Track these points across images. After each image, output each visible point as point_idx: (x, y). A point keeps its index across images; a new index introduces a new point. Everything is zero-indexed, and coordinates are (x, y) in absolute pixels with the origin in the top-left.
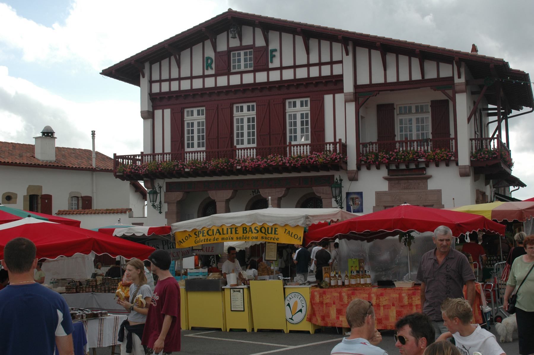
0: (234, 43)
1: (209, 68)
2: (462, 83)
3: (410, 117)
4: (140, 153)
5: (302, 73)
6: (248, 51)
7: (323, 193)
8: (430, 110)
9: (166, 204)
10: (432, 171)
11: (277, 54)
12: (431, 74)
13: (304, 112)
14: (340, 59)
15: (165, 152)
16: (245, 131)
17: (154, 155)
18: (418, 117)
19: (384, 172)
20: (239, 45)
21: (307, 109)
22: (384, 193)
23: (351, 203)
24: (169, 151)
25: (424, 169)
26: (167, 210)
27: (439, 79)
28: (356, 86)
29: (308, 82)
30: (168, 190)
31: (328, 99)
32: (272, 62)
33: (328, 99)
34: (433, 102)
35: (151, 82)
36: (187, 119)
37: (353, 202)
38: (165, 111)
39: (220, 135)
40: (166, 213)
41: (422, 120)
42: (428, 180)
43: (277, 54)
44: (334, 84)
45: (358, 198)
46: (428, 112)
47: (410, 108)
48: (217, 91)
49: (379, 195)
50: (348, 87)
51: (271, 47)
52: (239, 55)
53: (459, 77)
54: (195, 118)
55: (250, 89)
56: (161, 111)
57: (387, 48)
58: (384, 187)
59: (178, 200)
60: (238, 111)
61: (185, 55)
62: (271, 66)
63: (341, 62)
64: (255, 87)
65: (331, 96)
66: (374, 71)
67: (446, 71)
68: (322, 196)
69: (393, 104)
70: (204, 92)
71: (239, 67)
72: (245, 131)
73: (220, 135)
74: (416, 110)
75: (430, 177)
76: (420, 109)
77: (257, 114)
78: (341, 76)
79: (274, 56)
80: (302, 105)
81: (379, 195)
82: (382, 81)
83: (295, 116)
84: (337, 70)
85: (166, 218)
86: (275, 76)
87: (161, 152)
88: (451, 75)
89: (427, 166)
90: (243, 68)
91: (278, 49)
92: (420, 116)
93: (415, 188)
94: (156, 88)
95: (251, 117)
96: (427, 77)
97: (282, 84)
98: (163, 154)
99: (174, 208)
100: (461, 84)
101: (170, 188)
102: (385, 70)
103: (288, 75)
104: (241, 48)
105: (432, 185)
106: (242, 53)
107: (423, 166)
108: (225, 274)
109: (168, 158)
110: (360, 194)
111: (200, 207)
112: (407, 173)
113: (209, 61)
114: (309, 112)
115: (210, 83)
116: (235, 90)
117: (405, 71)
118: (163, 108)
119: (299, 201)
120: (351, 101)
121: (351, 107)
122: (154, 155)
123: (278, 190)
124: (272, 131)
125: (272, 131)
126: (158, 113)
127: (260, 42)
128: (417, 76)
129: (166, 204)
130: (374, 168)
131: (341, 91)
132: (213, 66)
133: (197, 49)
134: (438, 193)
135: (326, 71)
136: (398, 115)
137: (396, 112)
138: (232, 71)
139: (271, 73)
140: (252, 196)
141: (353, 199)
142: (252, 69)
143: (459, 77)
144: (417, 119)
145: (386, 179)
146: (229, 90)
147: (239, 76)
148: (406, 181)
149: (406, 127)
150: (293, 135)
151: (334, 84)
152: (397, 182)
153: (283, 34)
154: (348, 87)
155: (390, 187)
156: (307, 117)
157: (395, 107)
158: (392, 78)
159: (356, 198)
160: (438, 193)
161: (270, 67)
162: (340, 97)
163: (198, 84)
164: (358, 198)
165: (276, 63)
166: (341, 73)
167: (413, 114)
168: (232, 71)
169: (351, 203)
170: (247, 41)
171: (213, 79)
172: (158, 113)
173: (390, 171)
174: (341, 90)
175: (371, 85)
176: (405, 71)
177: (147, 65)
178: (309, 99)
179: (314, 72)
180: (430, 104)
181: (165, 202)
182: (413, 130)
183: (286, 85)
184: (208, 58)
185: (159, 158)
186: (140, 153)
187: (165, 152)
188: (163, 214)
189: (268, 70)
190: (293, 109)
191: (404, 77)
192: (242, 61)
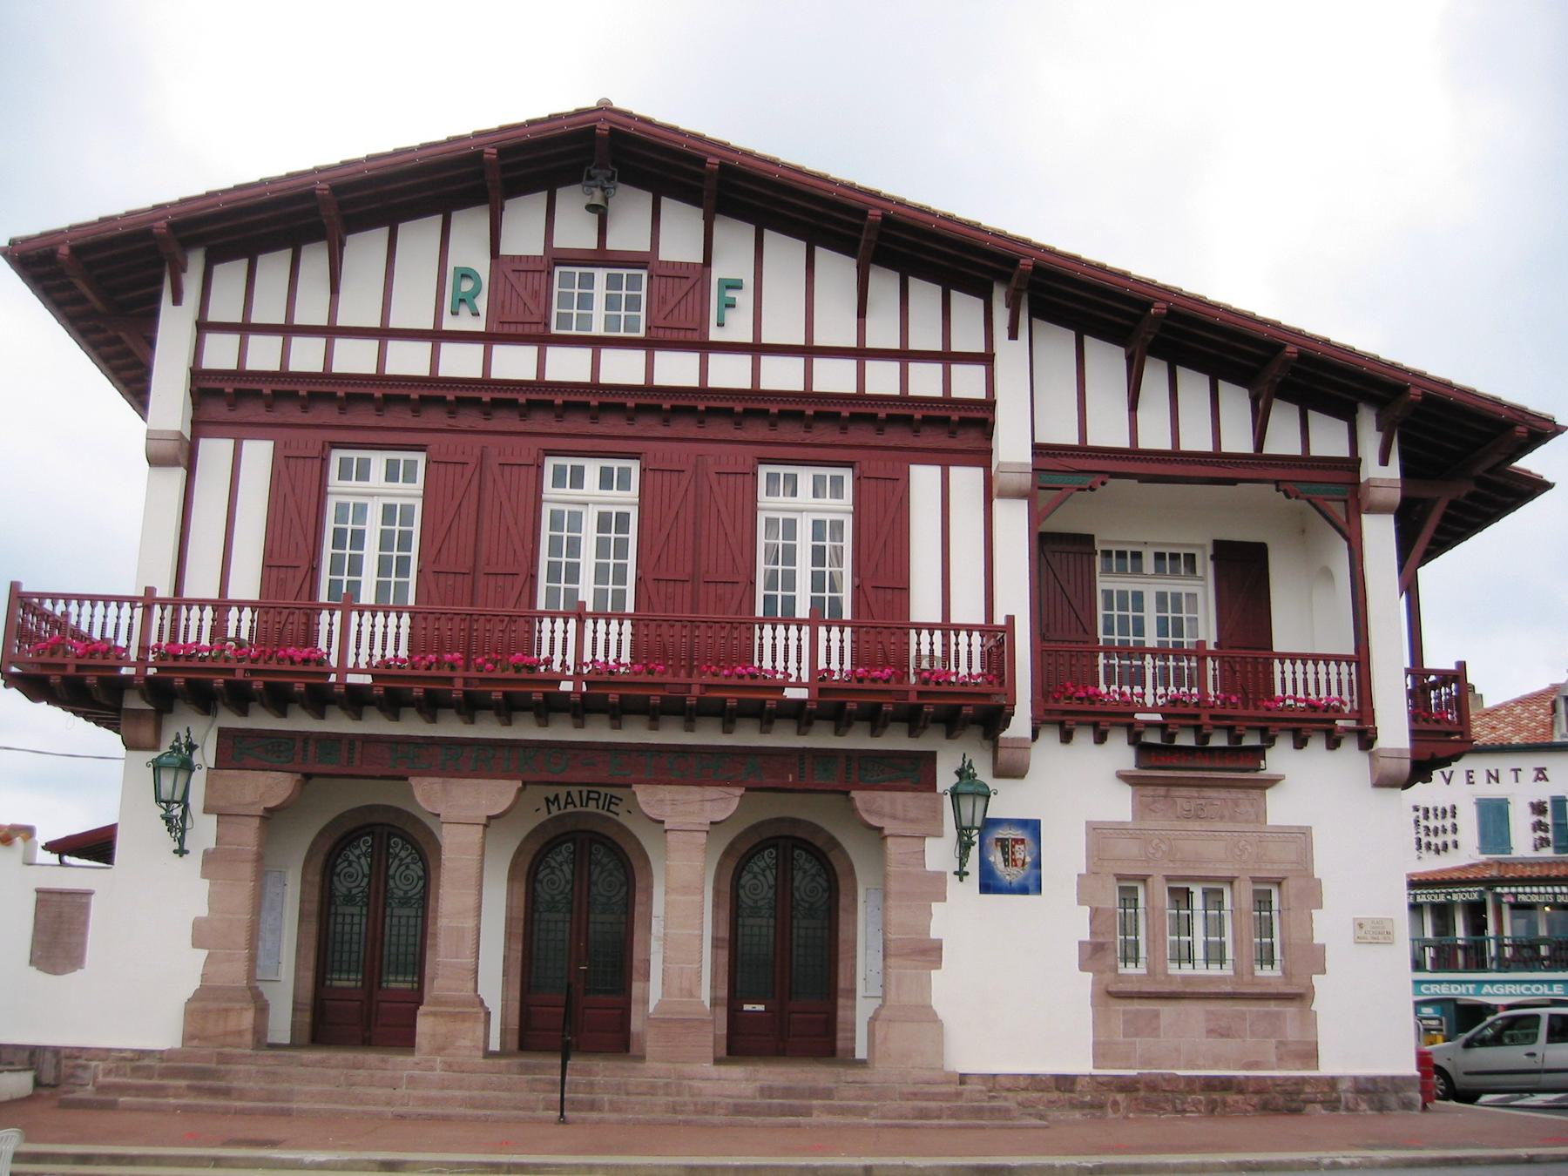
0: (576, 232)
2: (1391, 480)
3: (1138, 588)
5: (835, 377)
6: (625, 272)
7: (894, 817)
9: (214, 818)
10: (1280, 758)
11: (745, 299)
12: (1283, 439)
14: (981, 348)
15: (233, 594)
17: (178, 601)
18: (1162, 588)
19: (1119, 754)
20: (592, 244)
21: (840, 507)
22: (1118, 828)
23: (996, 858)
24: (253, 594)
25: (1258, 753)
26: (211, 844)
27: (1306, 461)
29: (858, 412)
30: (223, 761)
31: (924, 479)
33: (924, 479)
35: (204, 326)
36: (340, 489)
37: (1004, 853)
38: (249, 446)
39: (480, 557)
40: (208, 857)
41: (1177, 597)
42: (1268, 792)
44: (962, 430)
45: (1022, 841)
47: (1137, 556)
49: (1099, 833)
50: (1012, 446)
51: (718, 272)
52: (588, 281)
53: (1384, 461)
54: (378, 493)
56: (227, 445)
58: (1119, 805)
59: (271, 804)
61: (364, 251)
68: (890, 827)
73: (480, 557)
75: (1273, 782)
76: (1176, 562)
78: (989, 405)
79: (731, 305)
81: (1099, 833)
83: (790, 526)
84: (968, 383)
85: (204, 875)
86: (730, 373)
89: (1270, 741)
92: (1170, 586)
93: (1222, 818)
94: (221, 354)
95: (614, 510)
96: (1269, 449)
97: (753, 407)
98: (221, 606)
99: (248, 835)
100: (1387, 484)
101: (234, 752)
102: (1133, 407)
104: (602, 257)
105: (1280, 808)
106: (601, 275)
107: (1251, 740)
109: (241, 624)
110: (1033, 827)
112: (1205, 764)
115: (461, 362)
117: (1199, 417)
118: (239, 430)
119: (732, 845)
122: (178, 601)
123: (712, 792)
124: (695, 568)
125: (695, 568)
126: (215, 452)
128: (1238, 441)
130: (1083, 739)
132: (482, 303)
133: (419, 238)
134: (1301, 837)
135: (926, 381)
140: (543, 816)
141: (1003, 843)
143: (1384, 461)
144: (1161, 598)
145: (1125, 778)
146: (538, 399)
147: (585, 354)
148: (1194, 792)
149: (1123, 620)
152: (1162, 791)
153: (769, 235)
155: (1140, 809)
158: (1155, 437)
159: (1016, 841)
160: (1301, 837)
161: (712, 338)
163: (408, 360)
164: (1022, 841)
165: (738, 328)
166: (980, 394)
167: (1147, 576)
169: (996, 858)
170: (629, 234)
171: (478, 349)
173: (1144, 751)
174: (982, 456)
177: (195, 262)
179: (883, 379)
180: (1210, 551)
181: (206, 810)
184: (465, 274)
185: (197, 628)
187: (233, 594)
188: (194, 861)
189: (707, 348)
191: (1196, 439)
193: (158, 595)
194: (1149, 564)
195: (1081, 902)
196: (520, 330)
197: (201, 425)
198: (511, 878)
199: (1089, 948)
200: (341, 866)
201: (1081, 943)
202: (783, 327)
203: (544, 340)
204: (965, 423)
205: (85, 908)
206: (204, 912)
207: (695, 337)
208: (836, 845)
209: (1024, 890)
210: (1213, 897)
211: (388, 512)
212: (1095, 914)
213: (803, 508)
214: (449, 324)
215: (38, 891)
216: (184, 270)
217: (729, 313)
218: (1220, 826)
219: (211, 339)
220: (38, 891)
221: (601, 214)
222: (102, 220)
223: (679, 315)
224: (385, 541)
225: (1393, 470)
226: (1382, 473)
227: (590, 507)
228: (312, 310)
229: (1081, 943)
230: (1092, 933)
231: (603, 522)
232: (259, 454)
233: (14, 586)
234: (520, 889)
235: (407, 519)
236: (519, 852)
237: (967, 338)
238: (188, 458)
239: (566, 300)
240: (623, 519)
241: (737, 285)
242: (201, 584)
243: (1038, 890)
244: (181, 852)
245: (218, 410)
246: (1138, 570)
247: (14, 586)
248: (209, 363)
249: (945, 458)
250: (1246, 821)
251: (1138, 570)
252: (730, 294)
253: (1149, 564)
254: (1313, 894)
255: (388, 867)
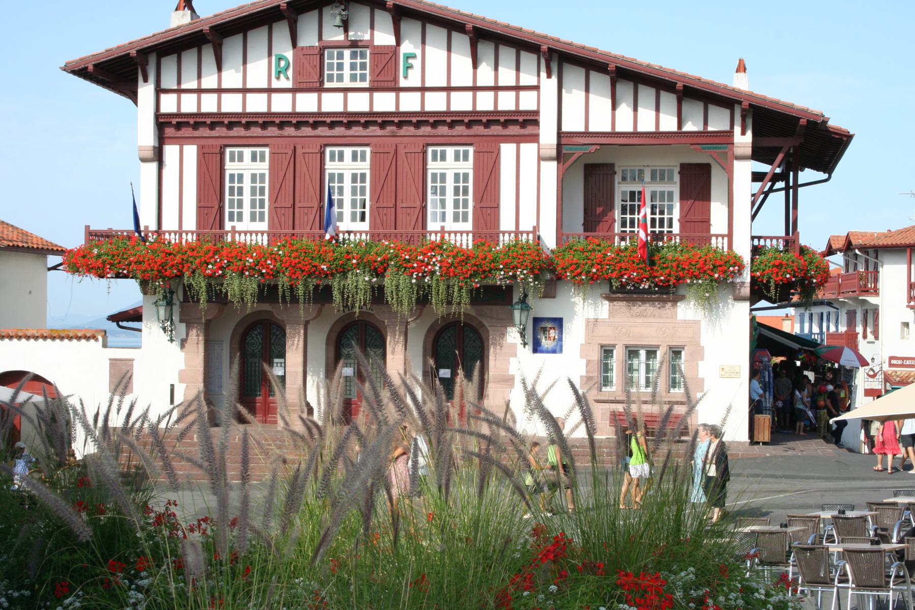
1: (282, 76)
4: (531, 229)
8: (677, 178)
9: (184, 325)
13: (258, 172)
14: (535, 84)
16: (247, 197)
21: (467, 167)
24: (193, 227)
28: (560, 134)
31: (507, 150)
32: (406, 77)
33: (507, 150)
34: (683, 166)
35: (159, 91)
38: (187, 148)
39: (300, 194)
43: (416, 63)
44: (524, 124)
46: (676, 183)
48: (298, 121)
50: (548, 135)
52: (340, 56)
53: (743, 133)
54: (248, 167)
55: (226, 122)
56: (176, 148)
57: (627, 77)
60: (435, 159)
62: (403, 83)
63: (537, 88)
64: (369, 119)
65: (177, 147)
66: (592, 111)
67: (719, 121)
69: (611, 166)
70: (267, 120)
71: (340, 78)
72: (247, 197)
73: (300, 194)
74: (652, 178)
76: (659, 176)
77: (272, 169)
79: (411, 67)
80: (457, 158)
82: (652, 128)
84: (528, 102)
86: (410, 103)
87: (176, 228)
88: (727, 128)
90: (347, 83)
91: (418, 52)
92: (659, 188)
94: (169, 104)
95: (359, 172)
97: (421, 120)
98: (180, 232)
100: (744, 146)
103: (436, 103)
108: (552, 442)
111: (237, 325)
113: (283, 63)
114: (267, 173)
115: (282, 104)
116: (247, 122)
117: (651, 117)
118: (181, 141)
120: (550, 159)
121: (551, 169)
127: (384, 38)
129: (184, 325)
131: (534, 138)
132: (290, 73)
135: (507, 102)
136: (619, 183)
137: (618, 178)
138: (327, 85)
139: (402, 95)
142: (366, 85)
143: (743, 133)
146: (317, 120)
150: (258, 210)
151: (524, 124)
154: (548, 135)
156: (262, 181)
157: (616, 169)
162: (529, 150)
165: (413, 79)
166: (535, 108)
168: (327, 85)
171: (289, 96)
172: (171, 151)
175: (635, 134)
176: (651, 117)
178: (471, 150)
180: (677, 170)
181: (181, 321)
182: (674, 211)
183: (466, 120)
186: (531, 229)
189: (398, 90)
190: (236, 164)
192: (345, 68)
193: (150, 229)
194: (647, 177)
195: (582, 357)
196: (308, 86)
197: (162, 140)
198: (327, 344)
199: (585, 379)
200: (249, 339)
201: (581, 377)
202: (436, 78)
203: (320, 89)
204: (524, 124)
205: (132, 365)
206: (183, 367)
207: (392, 85)
208: (484, 326)
209: (554, 352)
210: (651, 354)
211: (254, 178)
212: (588, 363)
213: (451, 165)
214: (275, 84)
215: (110, 360)
216: (147, 64)
217: (410, 71)
218: (652, 320)
219: (163, 97)
220: (110, 360)
221: (345, 26)
222: (107, 51)
223: (385, 74)
224: (253, 191)
225: (749, 137)
226: (743, 140)
227: (349, 168)
228: (209, 81)
229: (581, 377)
230: (587, 372)
231: (354, 178)
232: (191, 151)
233: (87, 227)
234: (332, 349)
235: (262, 180)
236: (331, 331)
237: (528, 79)
238: (158, 156)
239: (331, 67)
240: (363, 176)
241: (414, 56)
242: (170, 223)
243: (561, 351)
244: (172, 340)
245: (169, 131)
246: (641, 179)
247: (87, 227)
248: (163, 110)
249: (517, 139)
250: (667, 318)
251: (641, 179)
252: (410, 61)
253: (647, 177)
254: (699, 353)
255: (270, 339)
